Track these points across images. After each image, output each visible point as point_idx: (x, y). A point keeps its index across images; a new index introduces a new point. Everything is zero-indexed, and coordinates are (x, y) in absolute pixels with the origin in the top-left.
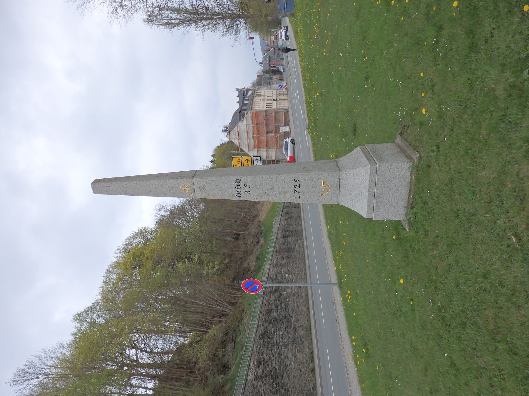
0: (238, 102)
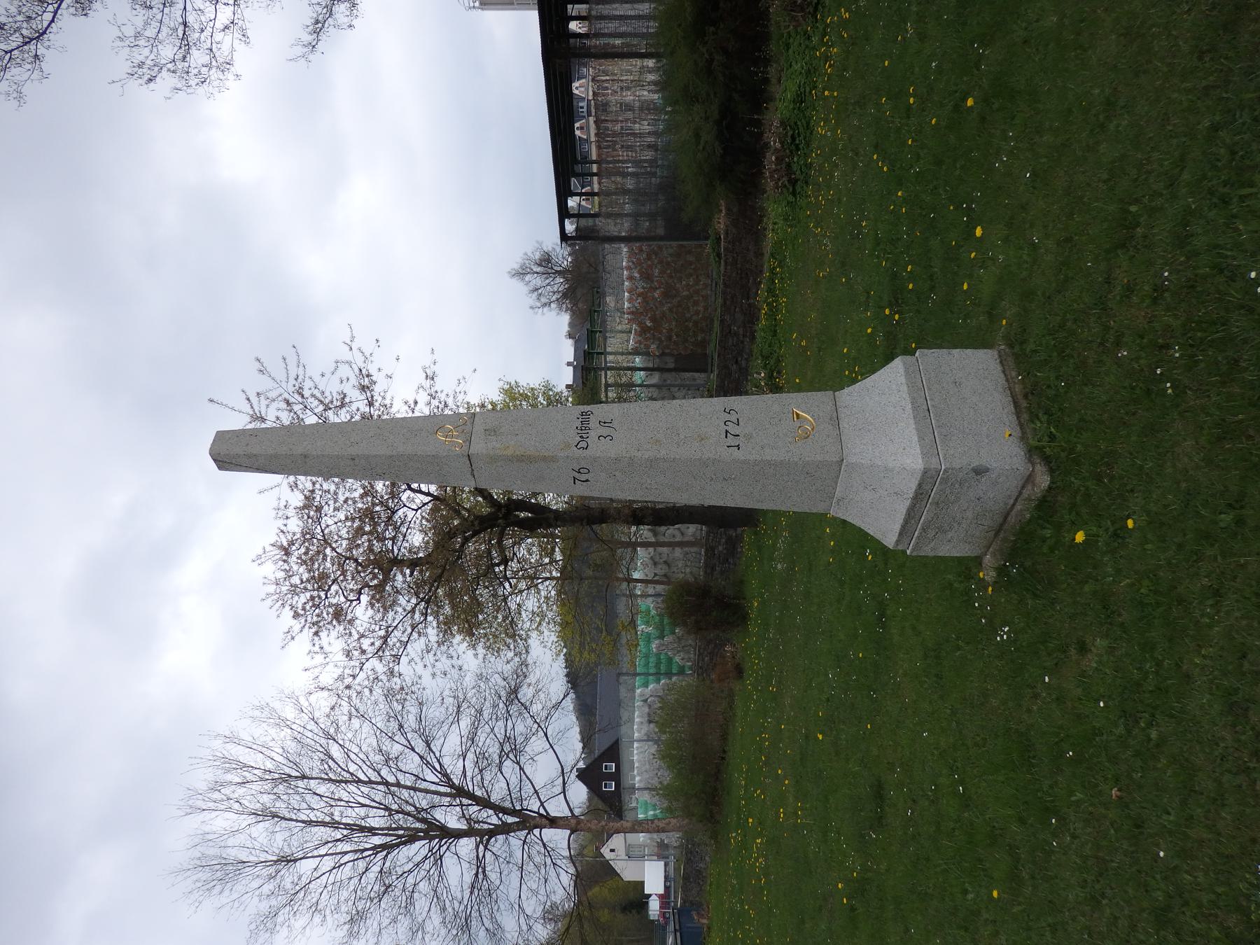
0: (569, 364)
